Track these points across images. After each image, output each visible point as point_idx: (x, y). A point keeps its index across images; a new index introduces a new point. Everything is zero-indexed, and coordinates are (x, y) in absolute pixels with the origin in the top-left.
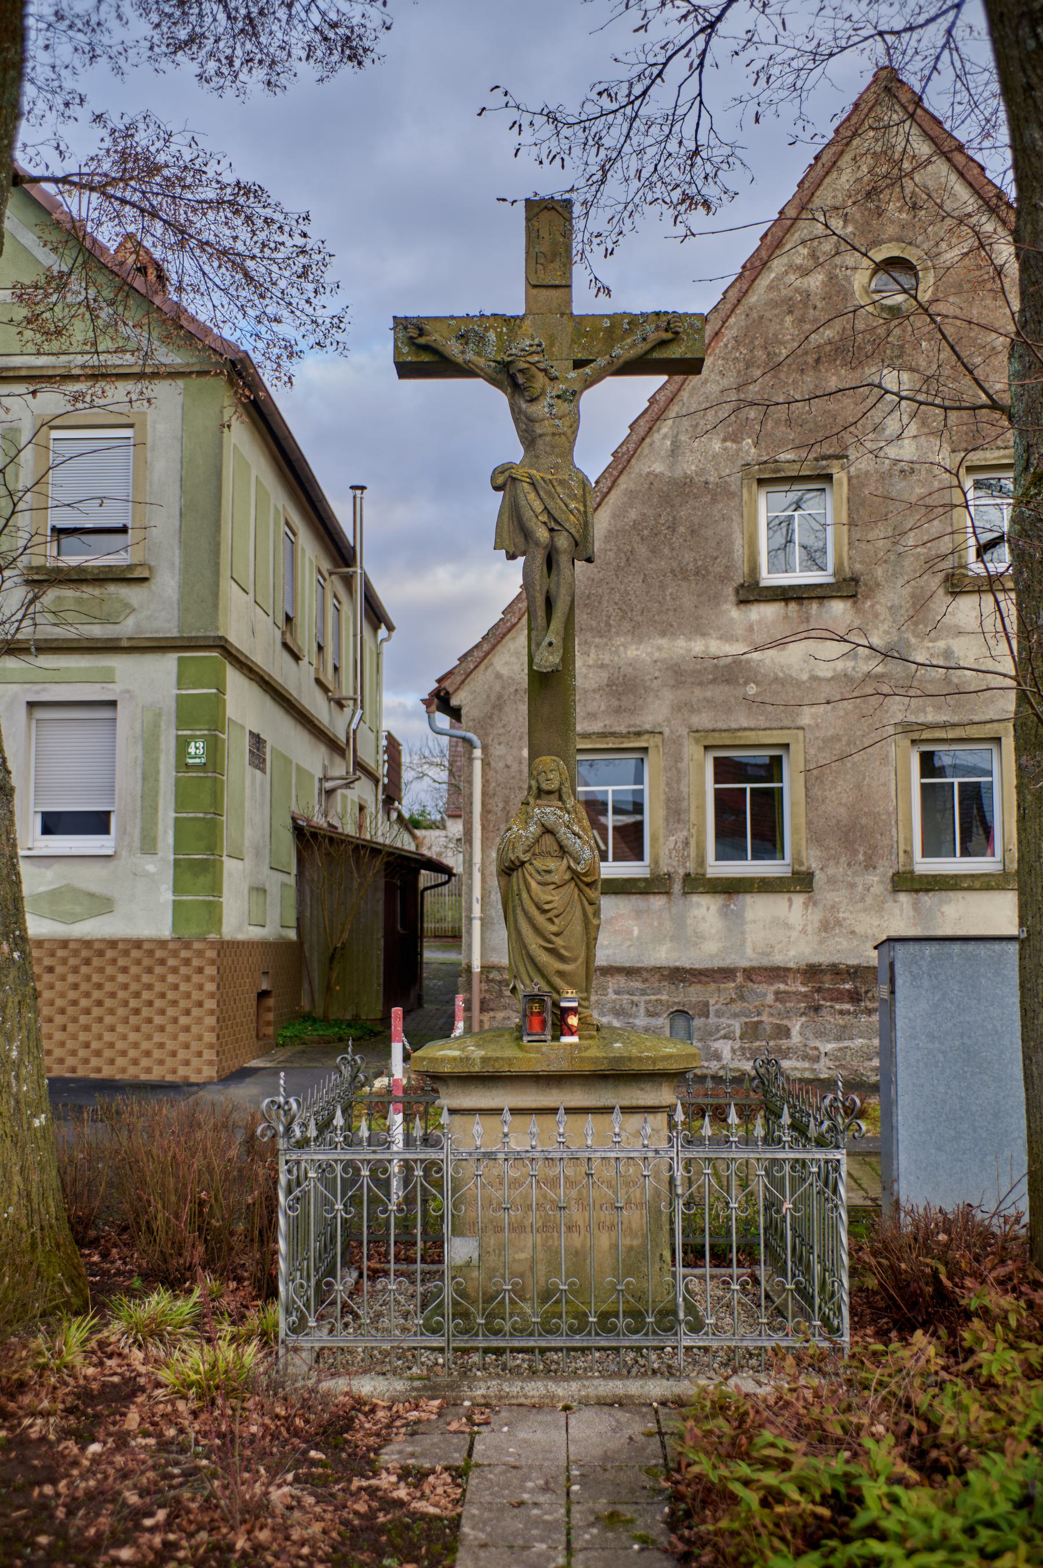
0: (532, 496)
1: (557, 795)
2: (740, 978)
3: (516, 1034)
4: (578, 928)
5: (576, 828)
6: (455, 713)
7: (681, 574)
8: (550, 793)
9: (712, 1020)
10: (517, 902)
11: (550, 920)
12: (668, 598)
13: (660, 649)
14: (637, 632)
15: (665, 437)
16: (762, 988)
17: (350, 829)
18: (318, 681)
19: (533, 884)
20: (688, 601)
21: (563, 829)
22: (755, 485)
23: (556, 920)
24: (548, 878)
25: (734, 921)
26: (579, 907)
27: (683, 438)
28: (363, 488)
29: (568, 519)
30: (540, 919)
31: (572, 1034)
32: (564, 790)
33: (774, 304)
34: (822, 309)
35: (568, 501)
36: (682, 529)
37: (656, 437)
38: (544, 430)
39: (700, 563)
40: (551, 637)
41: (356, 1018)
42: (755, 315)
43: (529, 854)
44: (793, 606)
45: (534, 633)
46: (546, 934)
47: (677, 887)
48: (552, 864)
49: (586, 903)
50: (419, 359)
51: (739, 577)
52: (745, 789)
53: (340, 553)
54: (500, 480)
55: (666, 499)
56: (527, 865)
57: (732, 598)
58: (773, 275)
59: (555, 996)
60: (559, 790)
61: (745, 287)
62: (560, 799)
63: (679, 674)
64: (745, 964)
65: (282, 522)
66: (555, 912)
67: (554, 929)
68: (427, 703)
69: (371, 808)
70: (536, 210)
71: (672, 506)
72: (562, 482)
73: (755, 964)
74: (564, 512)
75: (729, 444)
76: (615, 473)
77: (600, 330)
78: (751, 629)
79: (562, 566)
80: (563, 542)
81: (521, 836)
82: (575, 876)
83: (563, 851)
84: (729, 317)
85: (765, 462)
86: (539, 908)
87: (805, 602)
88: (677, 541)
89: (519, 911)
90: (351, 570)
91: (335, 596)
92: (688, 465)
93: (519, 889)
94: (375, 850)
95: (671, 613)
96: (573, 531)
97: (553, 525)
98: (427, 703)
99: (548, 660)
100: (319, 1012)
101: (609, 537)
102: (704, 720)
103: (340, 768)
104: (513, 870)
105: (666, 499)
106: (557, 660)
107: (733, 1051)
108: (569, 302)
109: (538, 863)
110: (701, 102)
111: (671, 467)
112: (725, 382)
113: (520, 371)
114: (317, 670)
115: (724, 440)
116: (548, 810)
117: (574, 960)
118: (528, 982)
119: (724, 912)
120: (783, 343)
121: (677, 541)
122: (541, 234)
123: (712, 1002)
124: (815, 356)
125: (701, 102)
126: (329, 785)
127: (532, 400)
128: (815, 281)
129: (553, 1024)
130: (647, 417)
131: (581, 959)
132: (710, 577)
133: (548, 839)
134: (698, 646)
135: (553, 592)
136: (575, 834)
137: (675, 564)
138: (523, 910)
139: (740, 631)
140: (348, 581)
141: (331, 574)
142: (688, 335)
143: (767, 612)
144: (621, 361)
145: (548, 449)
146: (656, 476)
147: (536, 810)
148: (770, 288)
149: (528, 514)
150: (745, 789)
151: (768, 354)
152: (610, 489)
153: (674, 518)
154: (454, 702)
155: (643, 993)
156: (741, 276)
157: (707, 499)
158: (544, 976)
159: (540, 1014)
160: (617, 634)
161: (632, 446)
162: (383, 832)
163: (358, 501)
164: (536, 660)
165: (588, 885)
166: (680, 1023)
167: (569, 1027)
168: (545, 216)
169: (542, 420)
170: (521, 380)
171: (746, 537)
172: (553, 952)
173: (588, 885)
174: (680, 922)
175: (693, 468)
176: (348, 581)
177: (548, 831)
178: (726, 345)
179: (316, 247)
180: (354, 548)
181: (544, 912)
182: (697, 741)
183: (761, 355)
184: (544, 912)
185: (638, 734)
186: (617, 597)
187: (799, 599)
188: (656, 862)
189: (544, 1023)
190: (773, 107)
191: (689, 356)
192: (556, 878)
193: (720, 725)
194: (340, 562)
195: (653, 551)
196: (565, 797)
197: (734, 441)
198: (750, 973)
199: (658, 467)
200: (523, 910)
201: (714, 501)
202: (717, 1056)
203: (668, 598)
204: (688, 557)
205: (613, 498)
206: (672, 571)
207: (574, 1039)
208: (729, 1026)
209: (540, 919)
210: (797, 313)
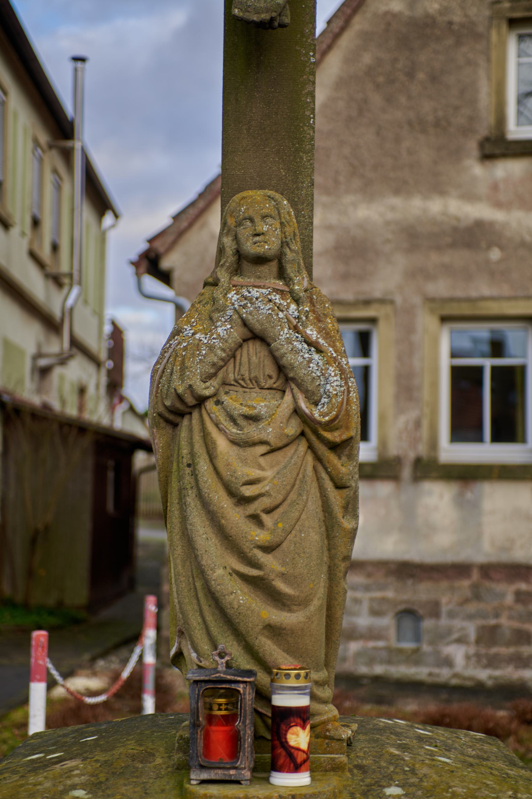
1: (274, 266)
2: (475, 575)
3: (178, 757)
4: (313, 536)
5: (312, 333)
6: (165, 277)
7: (419, 125)
8: (260, 260)
9: (444, 622)
10: (188, 479)
11: (255, 518)
13: (393, 209)
14: (368, 191)
16: (500, 587)
17: (72, 411)
18: (33, 256)
19: (222, 444)
20: (425, 155)
21: (285, 333)
22: (504, 27)
23: (265, 518)
24: (252, 431)
25: (469, 510)
26: (314, 491)
30: (234, 516)
31: (296, 768)
32: (290, 255)
36: (421, 76)
39: (440, 114)
41: (60, 604)
43: (215, 383)
46: (246, 547)
47: (407, 472)
48: (261, 403)
49: (329, 485)
51: (483, 130)
52: (479, 370)
53: (59, 127)
56: (210, 404)
59: (263, 678)
60: (280, 258)
62: (282, 274)
63: (414, 237)
64: (480, 559)
66: (266, 502)
67: (262, 536)
68: (136, 264)
69: (91, 390)
73: (493, 559)
76: (349, 11)
78: (495, 187)
81: (198, 346)
82: (309, 430)
83: (285, 376)
86: (231, 493)
89: (191, 499)
90: (68, 144)
93: (192, 454)
94: (81, 428)
98: (136, 264)
100: (19, 598)
102: (440, 288)
103: (55, 346)
104: (182, 415)
107: (468, 657)
109: (234, 402)
114: (31, 243)
116: (255, 293)
117: (303, 603)
118: (205, 646)
119: (460, 502)
123: (444, 600)
126: (43, 362)
129: (257, 737)
131: (318, 602)
133: (254, 352)
134: (435, 206)
136: (310, 344)
138: (200, 496)
139: (483, 189)
147: (233, 296)
150: (479, 370)
154: (165, 264)
155: (367, 588)
158: (239, 635)
159: (229, 719)
162: (99, 413)
163: (79, 73)
165: (334, 447)
166: (408, 623)
167: (290, 752)
172: (260, 585)
173: (334, 447)
174: (409, 511)
175: (436, 6)
176: (67, 155)
177: (255, 336)
181: (243, 501)
182: (432, 311)
184: (243, 501)
185: (367, 303)
186: (346, 151)
188: (383, 444)
189: (234, 743)
192: (269, 432)
193: (459, 293)
195: (389, 100)
196: (290, 270)
198: (488, 570)
200: (200, 496)
201: (458, 43)
202: (448, 662)
204: (427, 107)
205: (346, 40)
206: (410, 123)
207: (301, 780)
208: (463, 629)
209: (234, 516)
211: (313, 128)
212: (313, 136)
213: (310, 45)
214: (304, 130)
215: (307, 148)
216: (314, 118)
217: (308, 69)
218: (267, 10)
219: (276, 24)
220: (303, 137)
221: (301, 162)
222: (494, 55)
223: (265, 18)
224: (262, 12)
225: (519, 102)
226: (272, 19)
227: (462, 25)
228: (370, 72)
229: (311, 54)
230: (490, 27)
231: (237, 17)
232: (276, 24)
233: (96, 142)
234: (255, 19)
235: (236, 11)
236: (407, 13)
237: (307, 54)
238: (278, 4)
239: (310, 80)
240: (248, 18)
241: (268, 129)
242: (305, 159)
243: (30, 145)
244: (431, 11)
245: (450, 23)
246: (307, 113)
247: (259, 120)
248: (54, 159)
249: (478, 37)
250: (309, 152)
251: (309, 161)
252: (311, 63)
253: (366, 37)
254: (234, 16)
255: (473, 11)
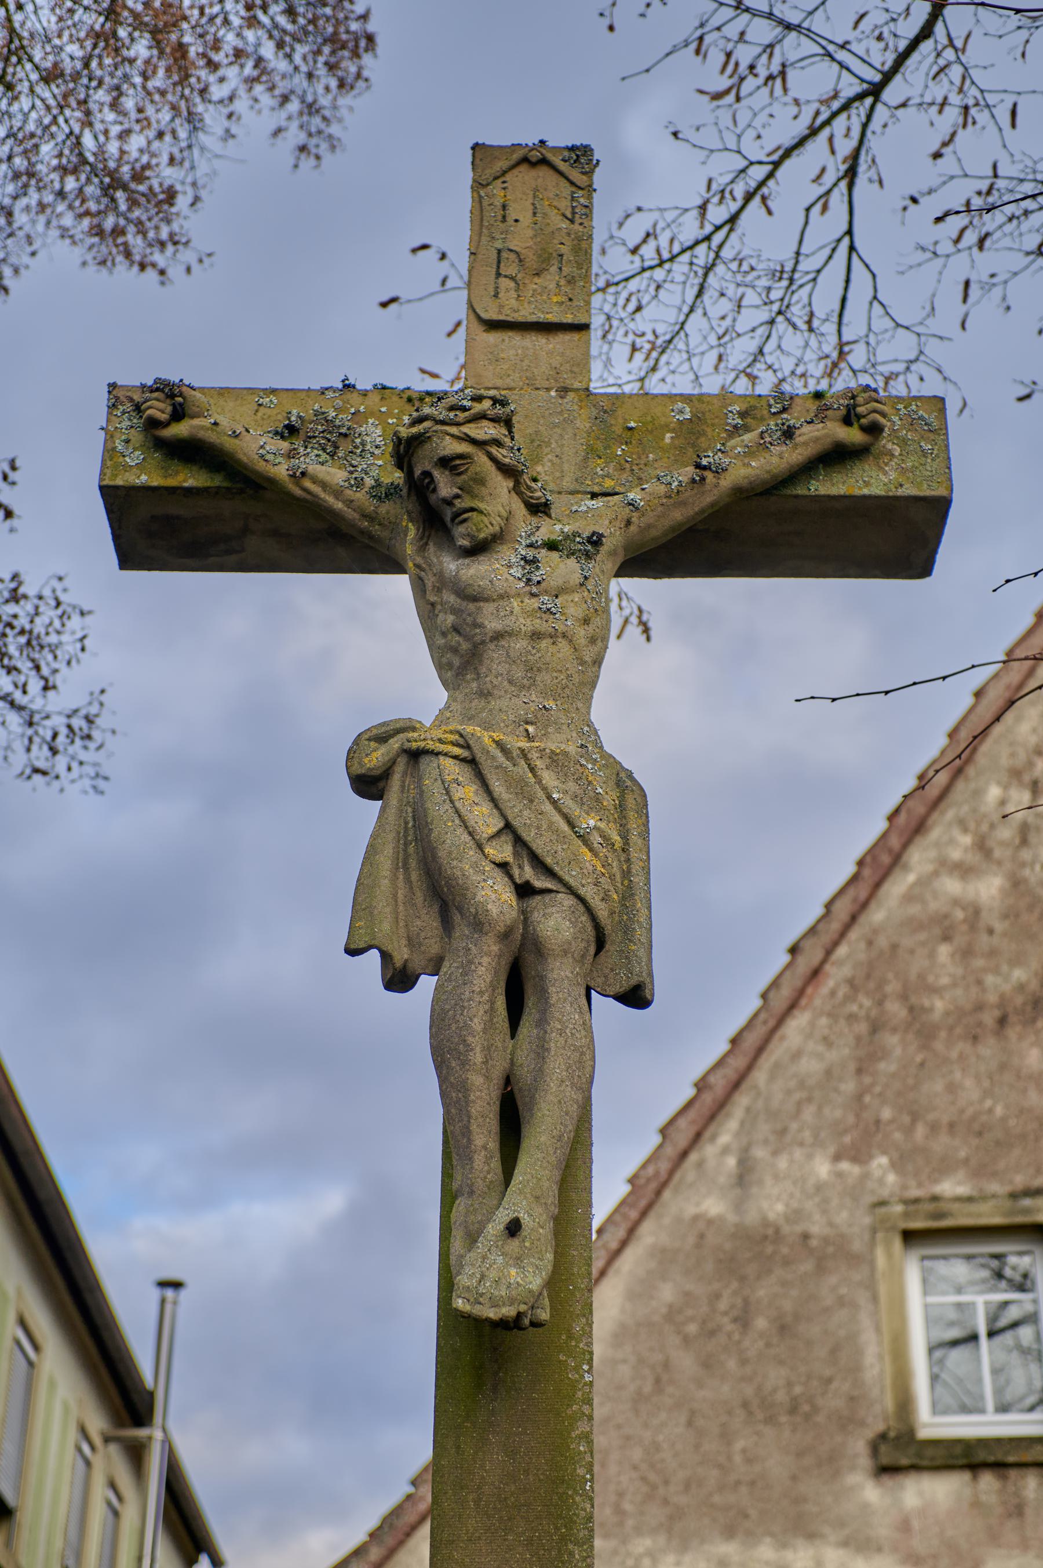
0: (467, 792)
7: (762, 1410)
12: (738, 1459)
15: (726, 1151)
20: (777, 1465)
22: (897, 1243)
27: (760, 1153)
28: (177, 1285)
29: (574, 860)
33: (915, 925)
34: (1005, 934)
35: (574, 810)
36: (761, 1323)
37: (709, 1151)
38: (510, 623)
39: (798, 1390)
40: (518, 1204)
42: (882, 942)
44: (988, 1480)
45: (461, 1205)
50: (171, 482)
54: (375, 758)
55: (729, 1266)
57: (865, 1461)
58: (911, 878)
61: (863, 895)
65: (11, 1318)
70: (502, 164)
71: (743, 1279)
72: (555, 760)
74: (562, 839)
75: (845, 1166)
76: (634, 1214)
77: (666, 427)
78: (905, 1526)
79: (555, 994)
80: (557, 923)
84: (836, 944)
85: (916, 1201)
87: (1013, 1473)
88: (753, 1345)
90: (142, 1433)
91: (112, 1485)
92: (772, 1204)
95: (744, 1490)
96: (588, 891)
97: (527, 873)
99: (508, 1279)
101: (620, 1335)
105: (729, 1266)
106: (536, 1282)
108: (583, 364)
110: (852, 248)
111: (738, 1206)
112: (833, 1056)
113: (445, 462)
115: (837, 1158)
120: (935, 990)
121: (753, 1345)
122: (512, 215)
124: (997, 1013)
125: (852, 248)
127: (478, 549)
128: (989, 889)
130: (692, 1114)
132: (820, 1418)
135: (525, 1074)
137: (749, 1391)
139: (883, 1529)
140: (136, 1454)
141: (107, 1440)
142: (903, 442)
143: (935, 1493)
144: (726, 482)
145: (519, 673)
146: (710, 1222)
148: (909, 898)
149: (451, 839)
151: (911, 1009)
152: (624, 1244)
153: (746, 1302)
156: (855, 879)
157: (807, 1266)
160: (638, 1531)
161: (664, 1166)
163: (168, 1308)
164: (463, 1280)
168: (524, 178)
169: (504, 596)
170: (445, 487)
171: (887, 1338)
175: (780, 1207)
176: (136, 1454)
178: (833, 993)
179: (47, 592)
180: (151, 1395)
183: (896, 1009)
186: (637, 1454)
187: (999, 1466)
190: (997, 292)
191: (909, 490)
194: (124, 1414)
195: (707, 1364)
197: (855, 1159)
199: (714, 1206)
201: (821, 1269)
203: (738, 1459)
204: (775, 1376)
206: (745, 1405)
210: (960, 940)
211: (591, 1499)
212: (592, 1513)
213: (584, 1354)
214: (574, 1502)
215: (581, 1534)
216: (592, 1480)
217: (580, 1394)
218: (512, 1301)
219: (526, 1322)
220: (574, 1514)
221: (570, 1562)
222: (883, 1289)
223: (507, 1314)
224: (504, 1305)
225: (931, 1350)
226: (520, 1315)
227: (826, 1241)
228: (671, 1315)
229: (586, 1367)
230: (872, 1244)
231: (461, 1311)
232: (526, 1322)
233: (190, 1431)
234: (491, 1315)
235: (459, 1303)
236: (732, 1218)
237: (577, 1369)
238: (530, 1291)
239: (583, 1413)
240: (479, 1314)
241: (513, 1499)
242: (577, 1556)
243: (73, 1435)
244: (771, 1216)
245: (806, 1237)
246: (581, 1471)
247: (497, 1483)
248: (111, 1461)
249: (854, 1260)
250: (584, 1543)
251: (584, 1559)
252: (585, 1384)
253: (664, 1257)
254: (456, 1310)
255: (842, 1217)
